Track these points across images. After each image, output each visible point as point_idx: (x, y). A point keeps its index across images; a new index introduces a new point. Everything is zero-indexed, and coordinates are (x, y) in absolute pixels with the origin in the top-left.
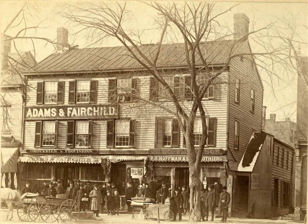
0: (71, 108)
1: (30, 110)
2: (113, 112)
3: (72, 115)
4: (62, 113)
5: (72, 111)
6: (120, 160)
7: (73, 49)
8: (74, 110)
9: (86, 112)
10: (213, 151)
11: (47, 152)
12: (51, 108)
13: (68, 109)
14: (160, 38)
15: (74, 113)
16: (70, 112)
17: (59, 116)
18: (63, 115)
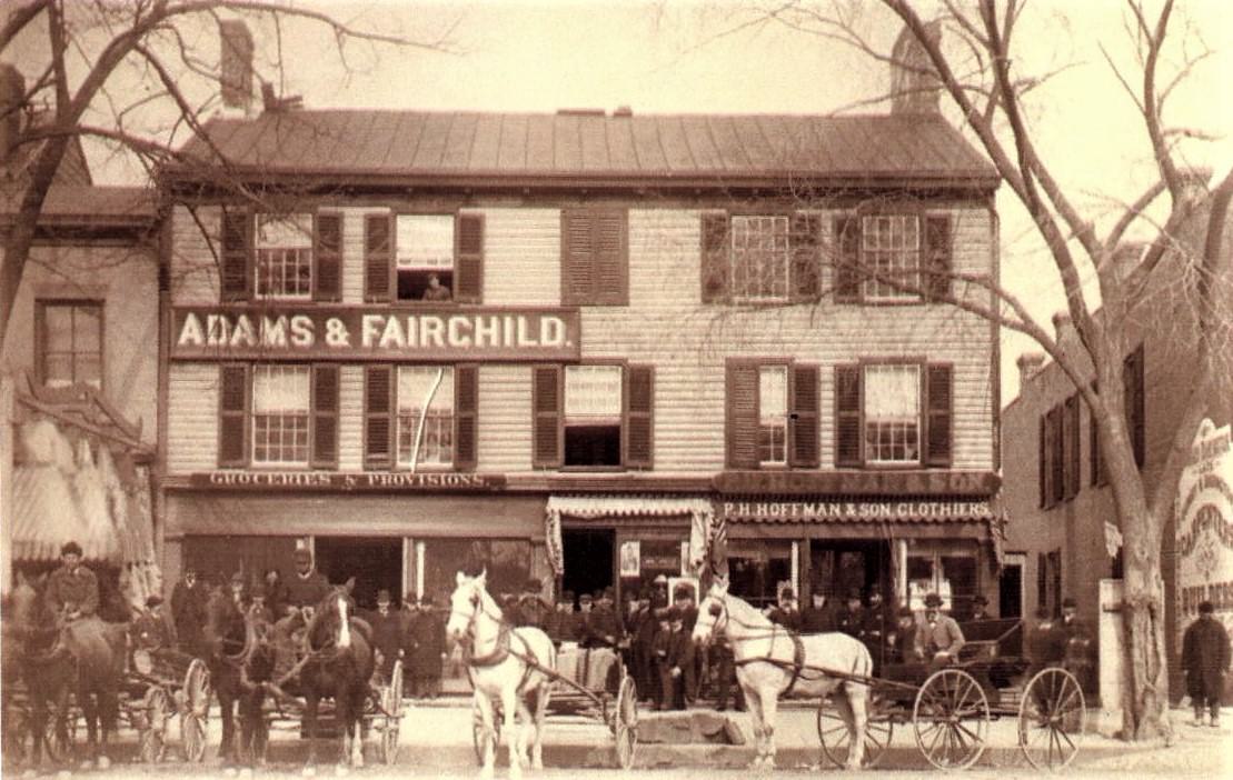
0: (378, 318)
1: (191, 321)
2: (553, 336)
3: (384, 342)
4: (337, 334)
5: (381, 327)
6: (589, 511)
7: (278, 108)
8: (393, 323)
9: (445, 336)
10: (963, 480)
11: (443, 482)
12: (291, 314)
13: (367, 319)
14: (159, 99)
15: (191, 336)
16: (375, 331)
17: (327, 346)
18: (346, 343)
